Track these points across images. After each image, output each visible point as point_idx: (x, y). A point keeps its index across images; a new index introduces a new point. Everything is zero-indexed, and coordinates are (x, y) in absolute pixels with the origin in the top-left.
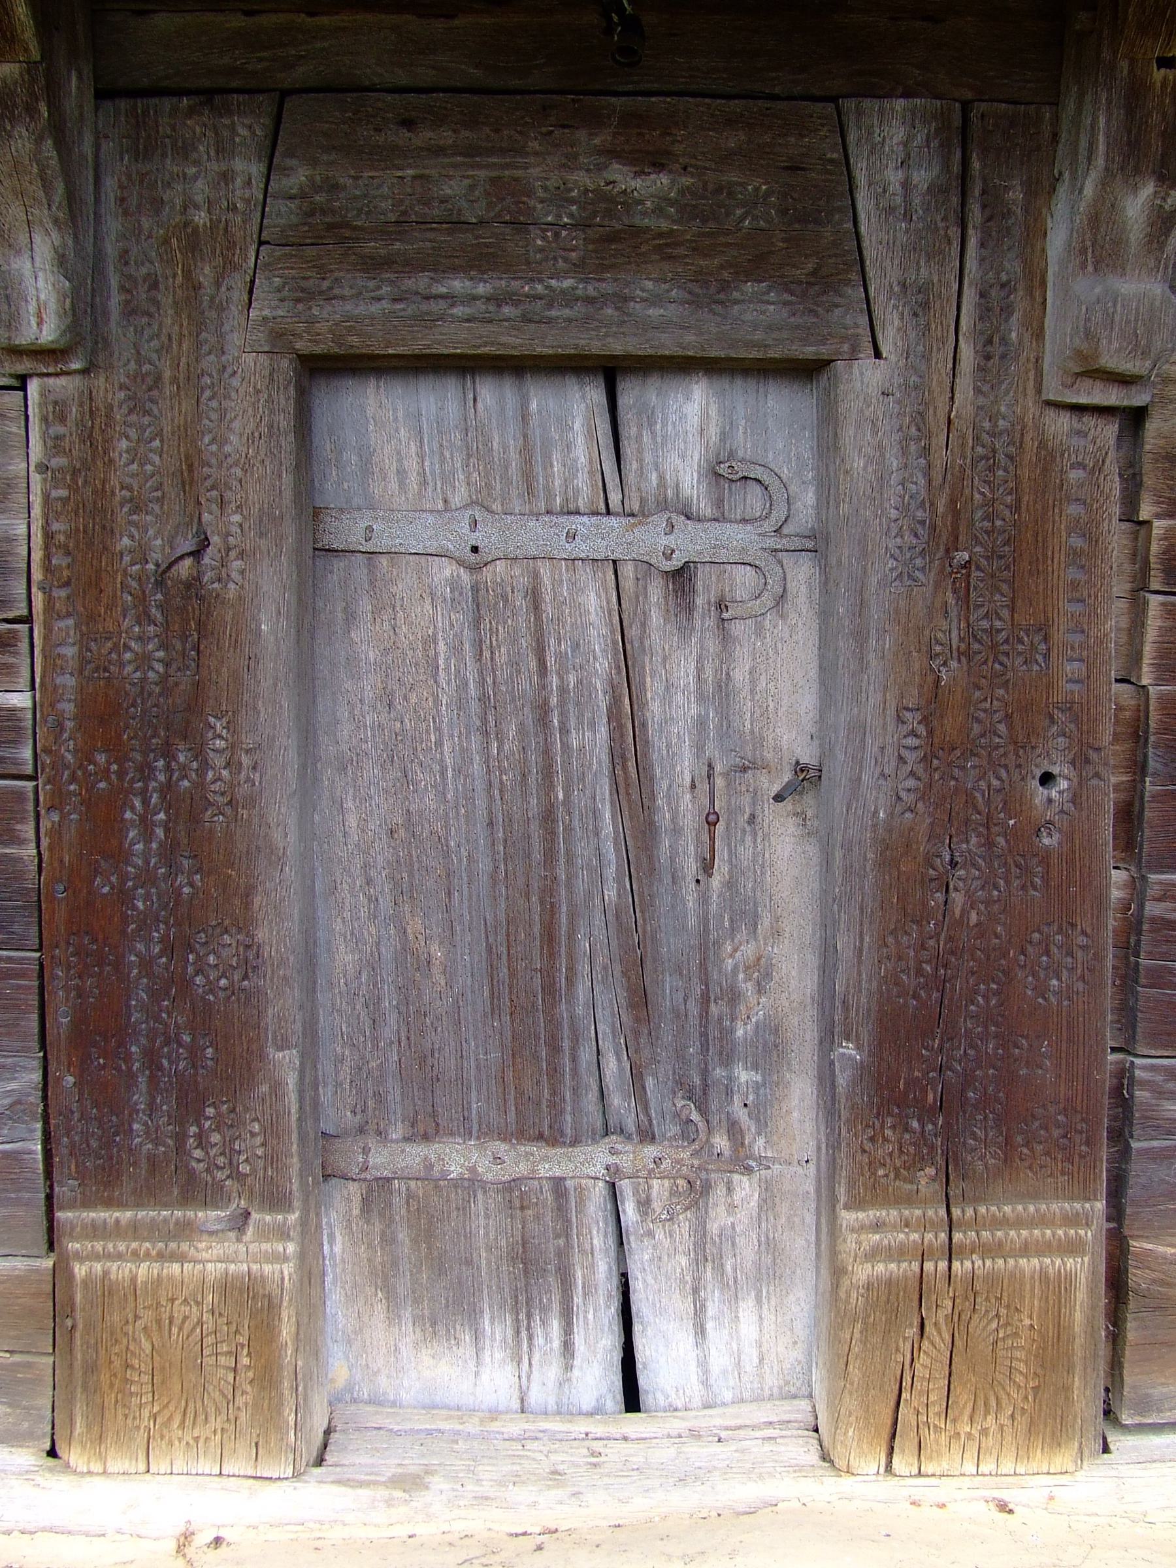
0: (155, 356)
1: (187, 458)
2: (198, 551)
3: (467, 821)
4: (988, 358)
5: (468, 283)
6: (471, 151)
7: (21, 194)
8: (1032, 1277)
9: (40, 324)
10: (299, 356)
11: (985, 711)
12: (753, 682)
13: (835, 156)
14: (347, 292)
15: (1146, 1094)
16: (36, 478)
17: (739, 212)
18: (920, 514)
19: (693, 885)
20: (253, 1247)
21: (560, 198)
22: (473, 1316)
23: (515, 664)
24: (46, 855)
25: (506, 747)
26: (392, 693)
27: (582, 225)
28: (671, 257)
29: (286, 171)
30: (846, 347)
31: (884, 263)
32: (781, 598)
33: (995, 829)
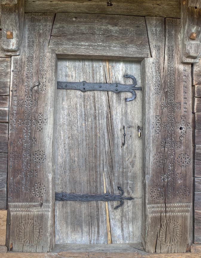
2: (38, 85)
3: (82, 136)
4: (170, 58)
6: (86, 22)
8: (180, 217)
9: (13, 46)
11: (170, 116)
12: (131, 112)
13: (144, 25)
14: (65, 44)
15: (197, 184)
16: (12, 73)
17: (129, 33)
19: (121, 147)
20: (43, 209)
21: (100, 30)
22: (81, 227)
23: (91, 108)
24: (9, 137)
25: (89, 123)
26: (70, 113)
27: (103, 34)
28: (117, 40)
30: (146, 55)
31: (153, 43)
32: (135, 98)
33: (172, 137)
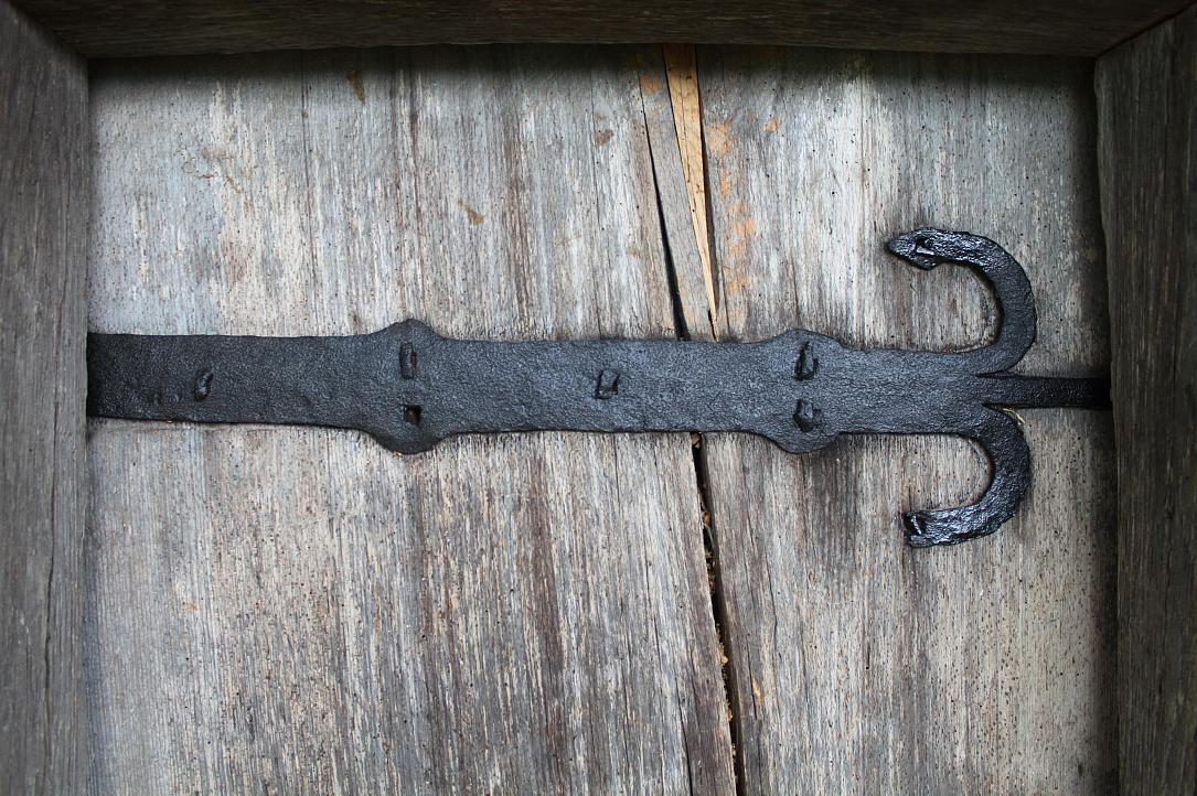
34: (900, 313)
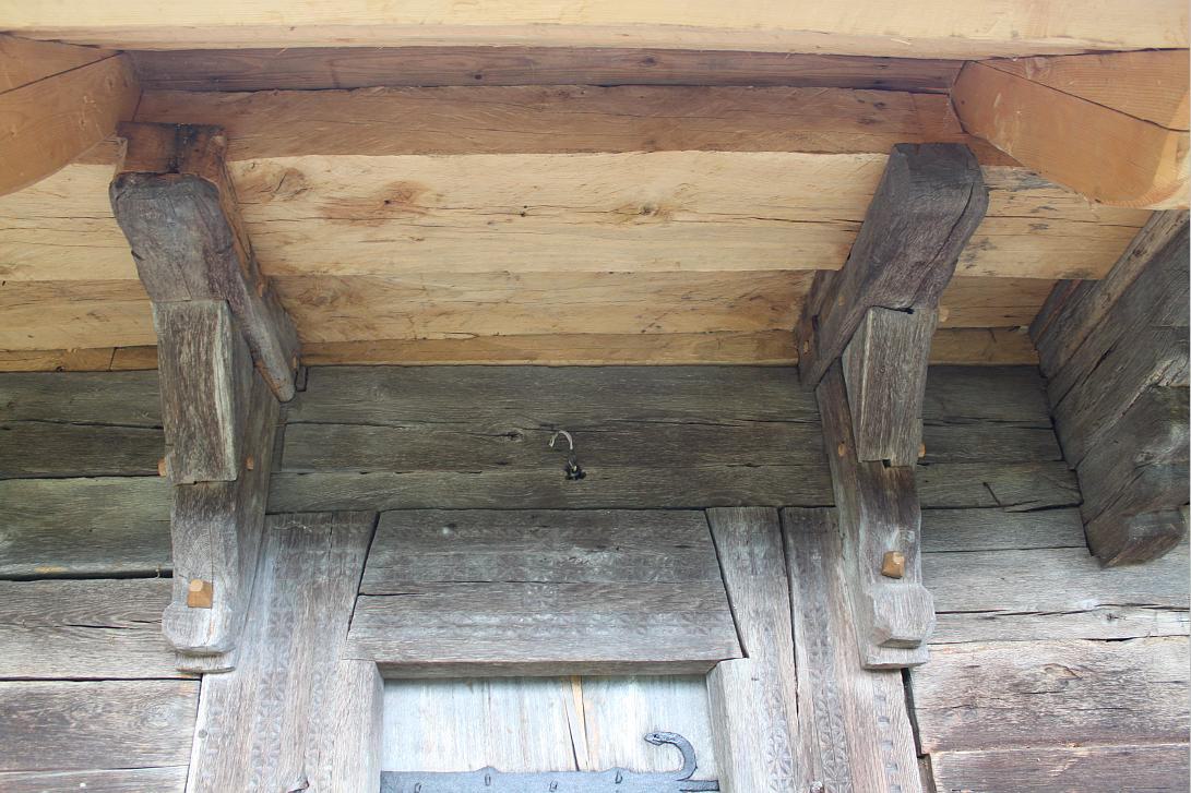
0: (285, 663)
1: (299, 727)
4: (815, 654)
5: (485, 618)
6: (488, 541)
7: (210, 555)
9: (209, 634)
10: (378, 664)
13: (706, 539)
17: (651, 573)
18: (786, 757)
29: (378, 552)
34: (651, 759)
